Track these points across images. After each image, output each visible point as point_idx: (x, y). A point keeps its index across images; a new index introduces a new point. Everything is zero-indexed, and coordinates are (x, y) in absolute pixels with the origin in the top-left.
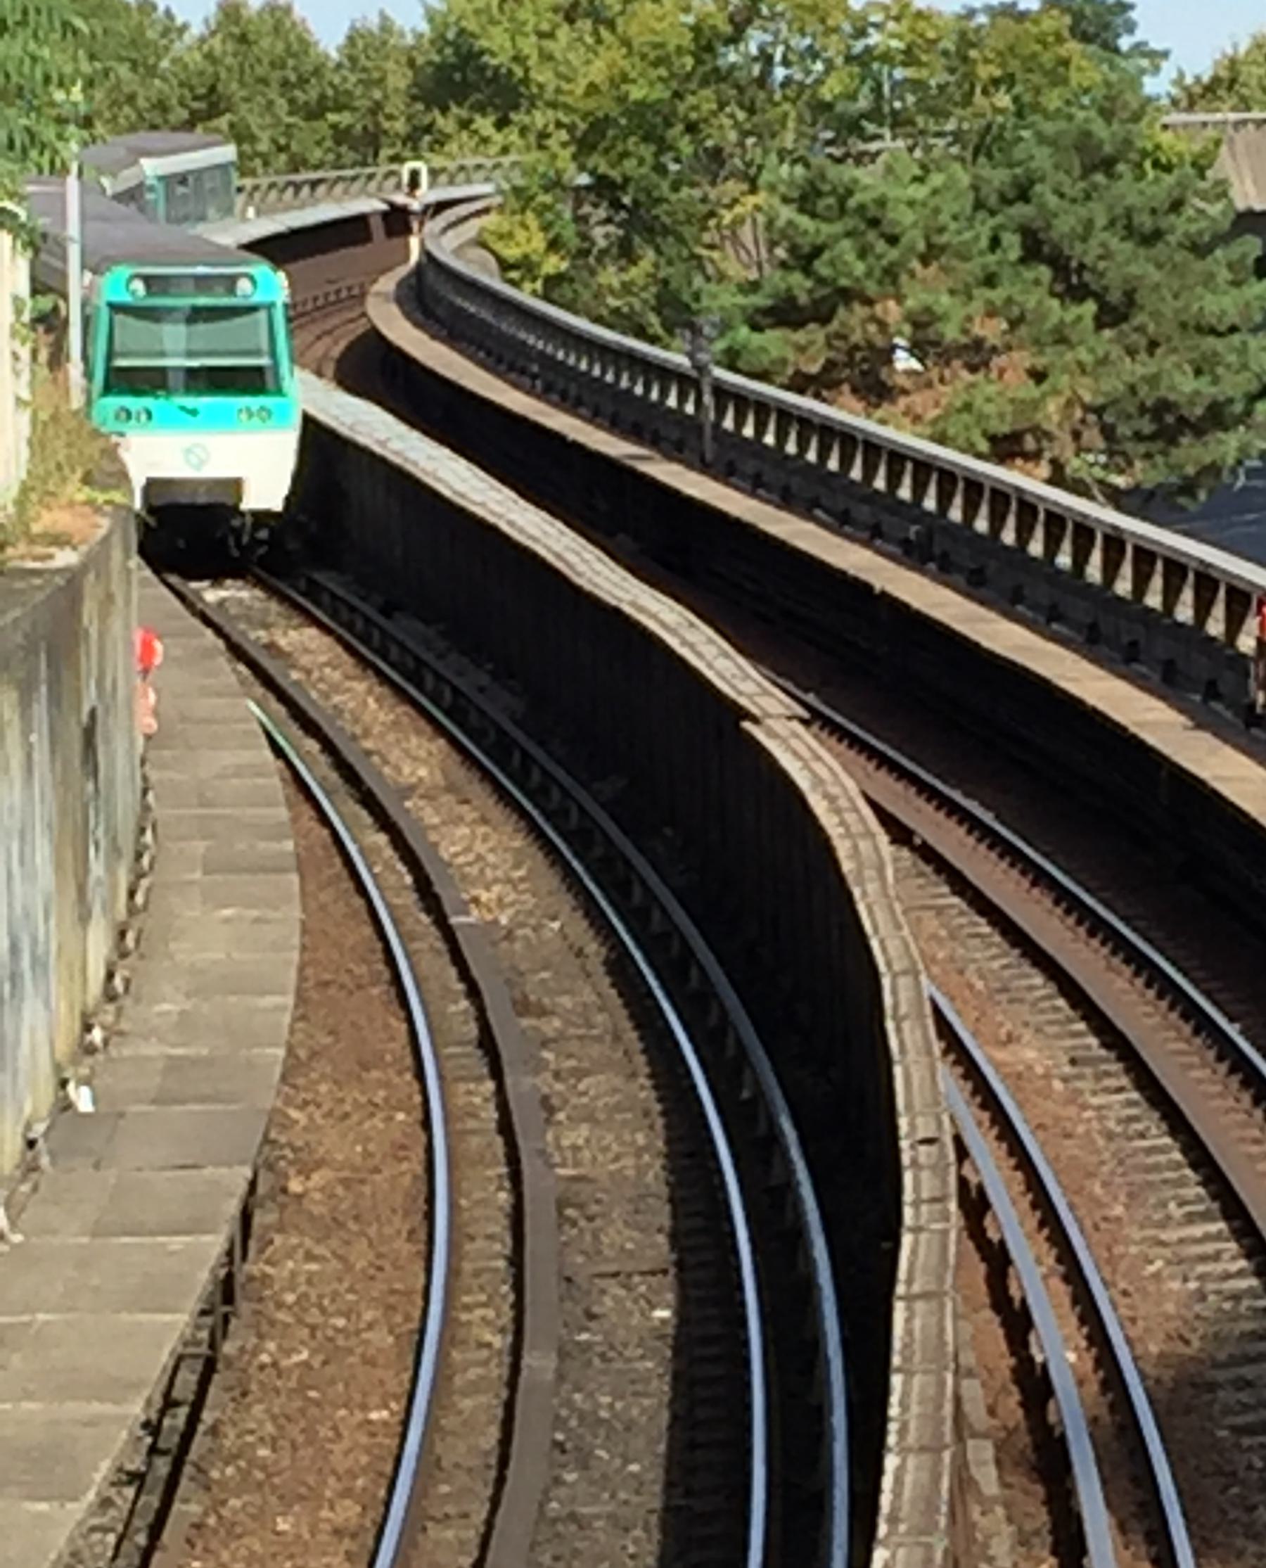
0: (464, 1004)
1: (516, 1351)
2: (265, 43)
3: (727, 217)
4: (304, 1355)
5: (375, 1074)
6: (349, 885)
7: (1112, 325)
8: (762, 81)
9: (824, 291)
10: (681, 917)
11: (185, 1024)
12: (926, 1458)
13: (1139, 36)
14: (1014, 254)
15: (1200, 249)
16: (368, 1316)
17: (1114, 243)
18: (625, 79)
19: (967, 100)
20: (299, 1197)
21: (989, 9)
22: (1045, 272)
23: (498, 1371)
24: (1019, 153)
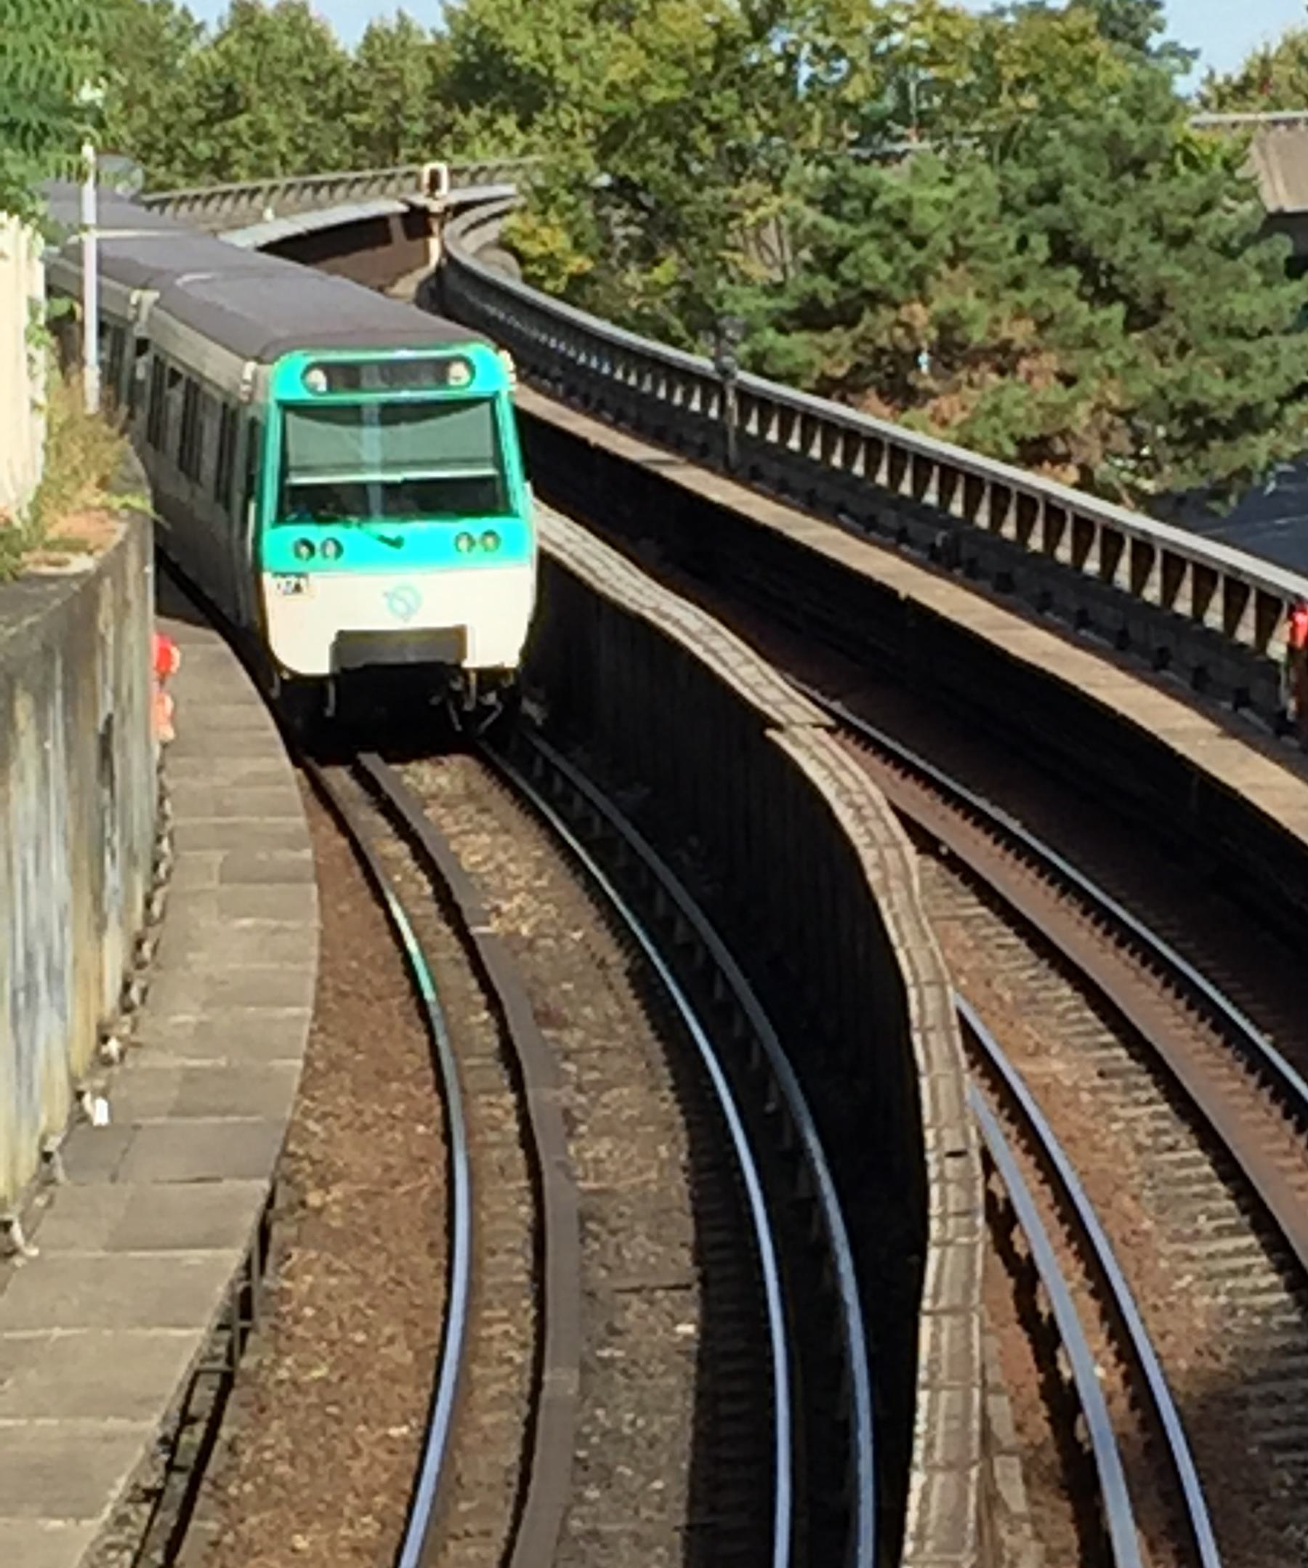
0: (485, 1015)
3: (750, 218)
5: (395, 1086)
8: (787, 81)
9: (852, 294)
12: (953, 1477)
13: (1168, 35)
16: (387, 1331)
20: (319, 1211)
21: (1016, 9)
22: (1073, 274)
23: (520, 1385)
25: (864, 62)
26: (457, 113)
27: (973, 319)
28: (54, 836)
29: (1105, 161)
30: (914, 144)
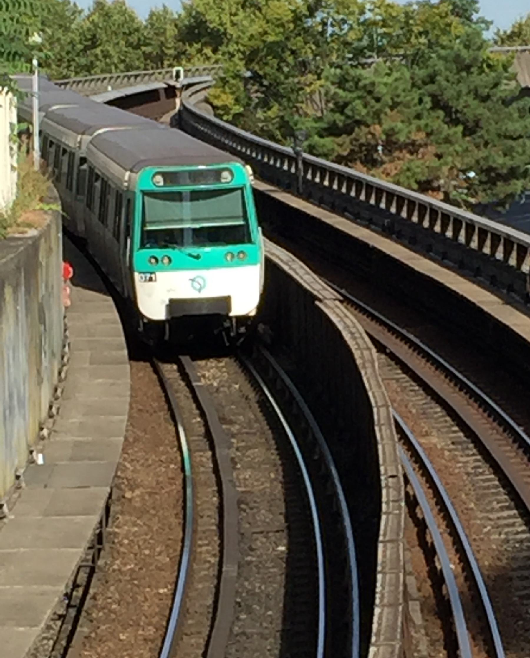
0: (199, 419)
1: (221, 564)
7: (470, 135)
8: (323, 33)
9: (349, 121)
14: (429, 105)
15: (506, 103)
16: (158, 549)
18: (266, 33)
20: (130, 500)
23: (214, 571)
28: (21, 344)
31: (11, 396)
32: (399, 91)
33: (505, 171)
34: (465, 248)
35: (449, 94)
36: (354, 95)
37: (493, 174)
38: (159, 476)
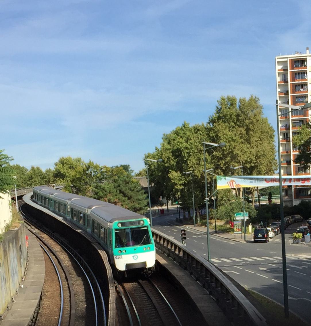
0: (64, 274)
1: (71, 310)
2: (37, 171)
3: (88, 189)
4: (48, 312)
5: (54, 282)
6: (50, 262)
7: (129, 200)
8: (91, 175)
9: (99, 197)
10: (86, 264)
11: (33, 278)
12: (112, 320)
13: (131, 169)
14: (119, 192)
15: (138, 191)
16: (55, 307)
17: (129, 191)
18: (76, 175)
19: (113, 177)
20: (47, 295)
21: (115, 167)
22: (122, 194)
23: (69, 312)
24: (119, 182)
25: (99, 173)
26: (56, 179)
27: (112, 199)
28: (15, 258)
29: (124, 183)
30: (105, 181)
31: (13, 271)
32: (111, 189)
33: (139, 208)
34: (170, 250)
35: (124, 189)
36: (100, 190)
37: (136, 209)
38: (179, 168)
